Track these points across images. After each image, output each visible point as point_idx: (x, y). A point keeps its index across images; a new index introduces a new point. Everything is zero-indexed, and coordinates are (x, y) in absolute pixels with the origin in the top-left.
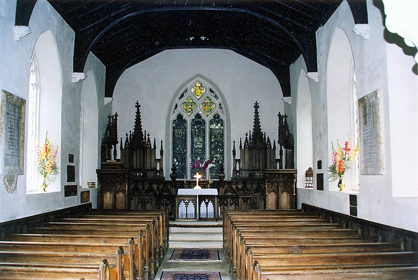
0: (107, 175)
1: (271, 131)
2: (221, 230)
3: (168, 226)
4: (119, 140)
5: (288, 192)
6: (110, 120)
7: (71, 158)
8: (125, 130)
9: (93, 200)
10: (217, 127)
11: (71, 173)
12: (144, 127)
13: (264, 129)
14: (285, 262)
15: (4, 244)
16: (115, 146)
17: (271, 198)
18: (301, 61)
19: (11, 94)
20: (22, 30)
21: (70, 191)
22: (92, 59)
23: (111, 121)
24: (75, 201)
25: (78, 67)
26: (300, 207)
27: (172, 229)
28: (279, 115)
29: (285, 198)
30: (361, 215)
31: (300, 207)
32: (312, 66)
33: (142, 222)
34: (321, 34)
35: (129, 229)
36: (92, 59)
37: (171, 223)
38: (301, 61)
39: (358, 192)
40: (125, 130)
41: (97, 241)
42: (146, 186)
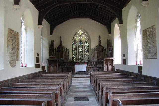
0: (50, 61)
1: (104, 44)
2: (89, 78)
3: (72, 77)
4: (55, 49)
5: (111, 65)
6: (51, 42)
7: (38, 55)
8: (56, 45)
9: (46, 69)
10: (87, 44)
11: (38, 60)
12: (63, 44)
13: (102, 44)
14: (126, 97)
15: (7, 89)
16: (53, 51)
17: (106, 67)
18: (117, 19)
19: (12, 30)
20: (17, 6)
21: (37, 66)
22: (44, 21)
23: (52, 43)
24: (40, 70)
25: (40, 23)
26: (116, 70)
27: (73, 78)
28: (107, 40)
29: (110, 67)
30: (145, 73)
31: (116, 70)
32: (121, 22)
33: (63, 77)
34: (124, 10)
35: (58, 80)
36: (44, 21)
37: (72, 76)
38: (117, 19)
39: (143, 65)
40: (56, 45)
41: (45, 86)
42: (64, 64)
